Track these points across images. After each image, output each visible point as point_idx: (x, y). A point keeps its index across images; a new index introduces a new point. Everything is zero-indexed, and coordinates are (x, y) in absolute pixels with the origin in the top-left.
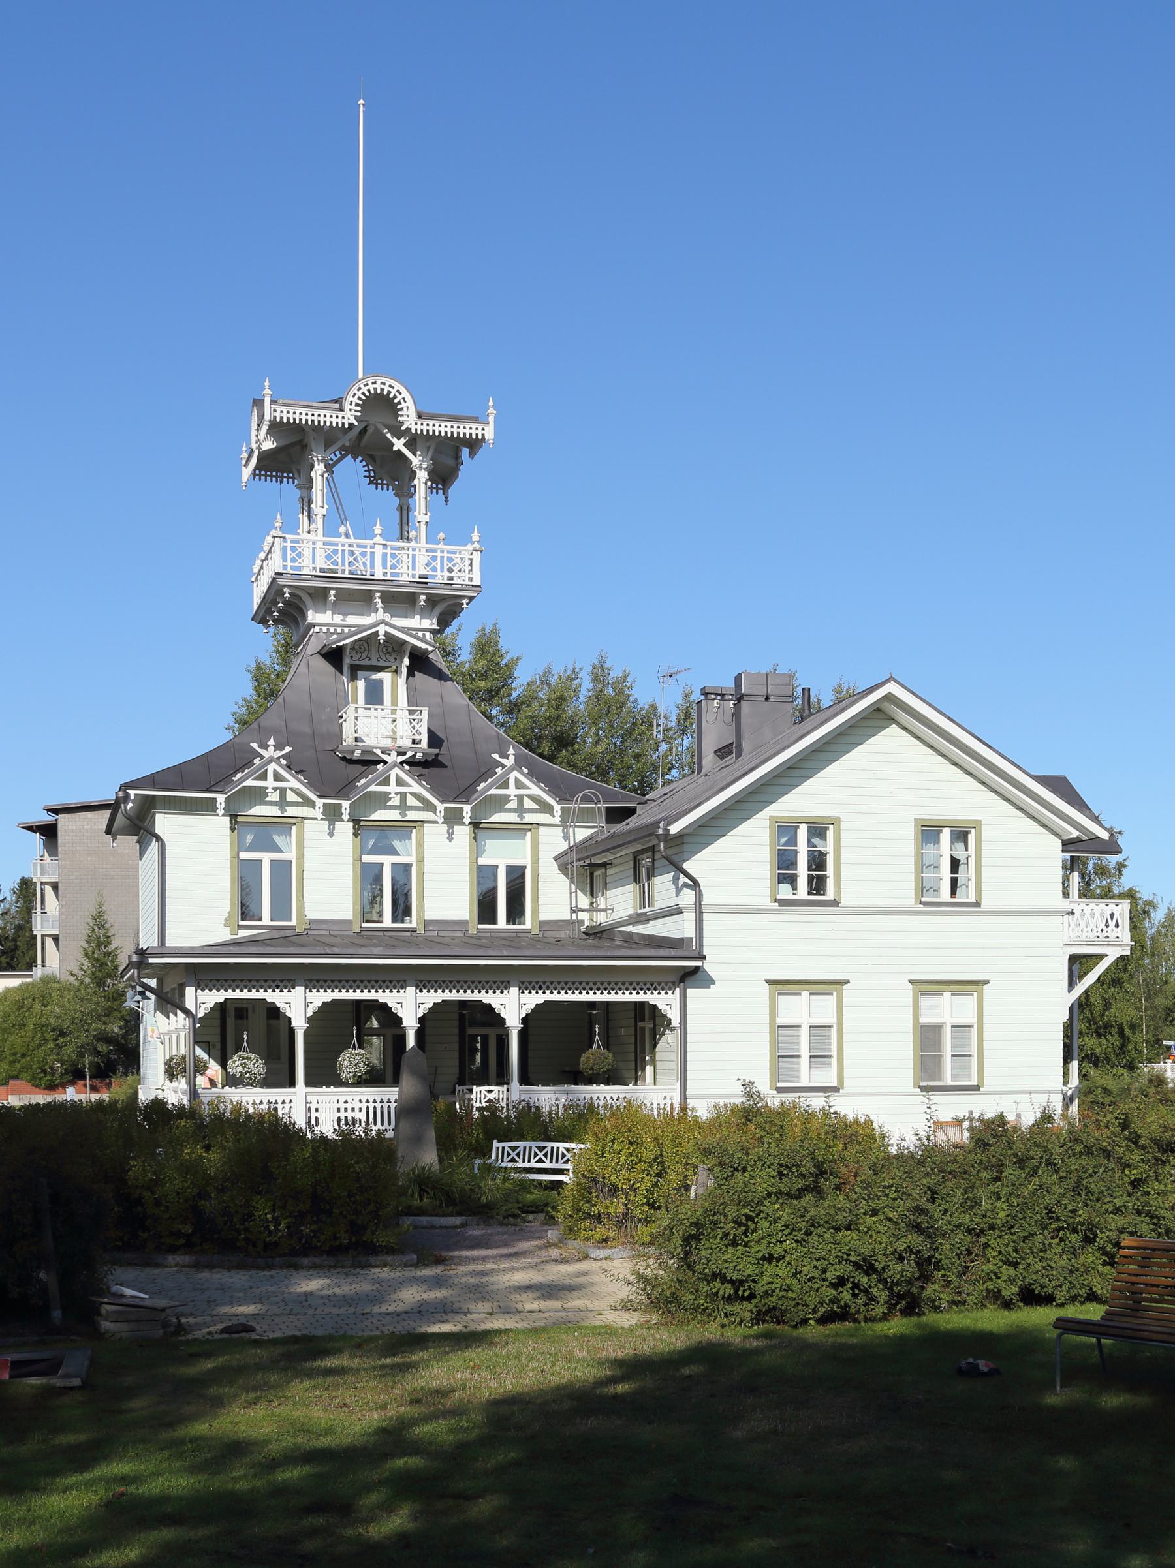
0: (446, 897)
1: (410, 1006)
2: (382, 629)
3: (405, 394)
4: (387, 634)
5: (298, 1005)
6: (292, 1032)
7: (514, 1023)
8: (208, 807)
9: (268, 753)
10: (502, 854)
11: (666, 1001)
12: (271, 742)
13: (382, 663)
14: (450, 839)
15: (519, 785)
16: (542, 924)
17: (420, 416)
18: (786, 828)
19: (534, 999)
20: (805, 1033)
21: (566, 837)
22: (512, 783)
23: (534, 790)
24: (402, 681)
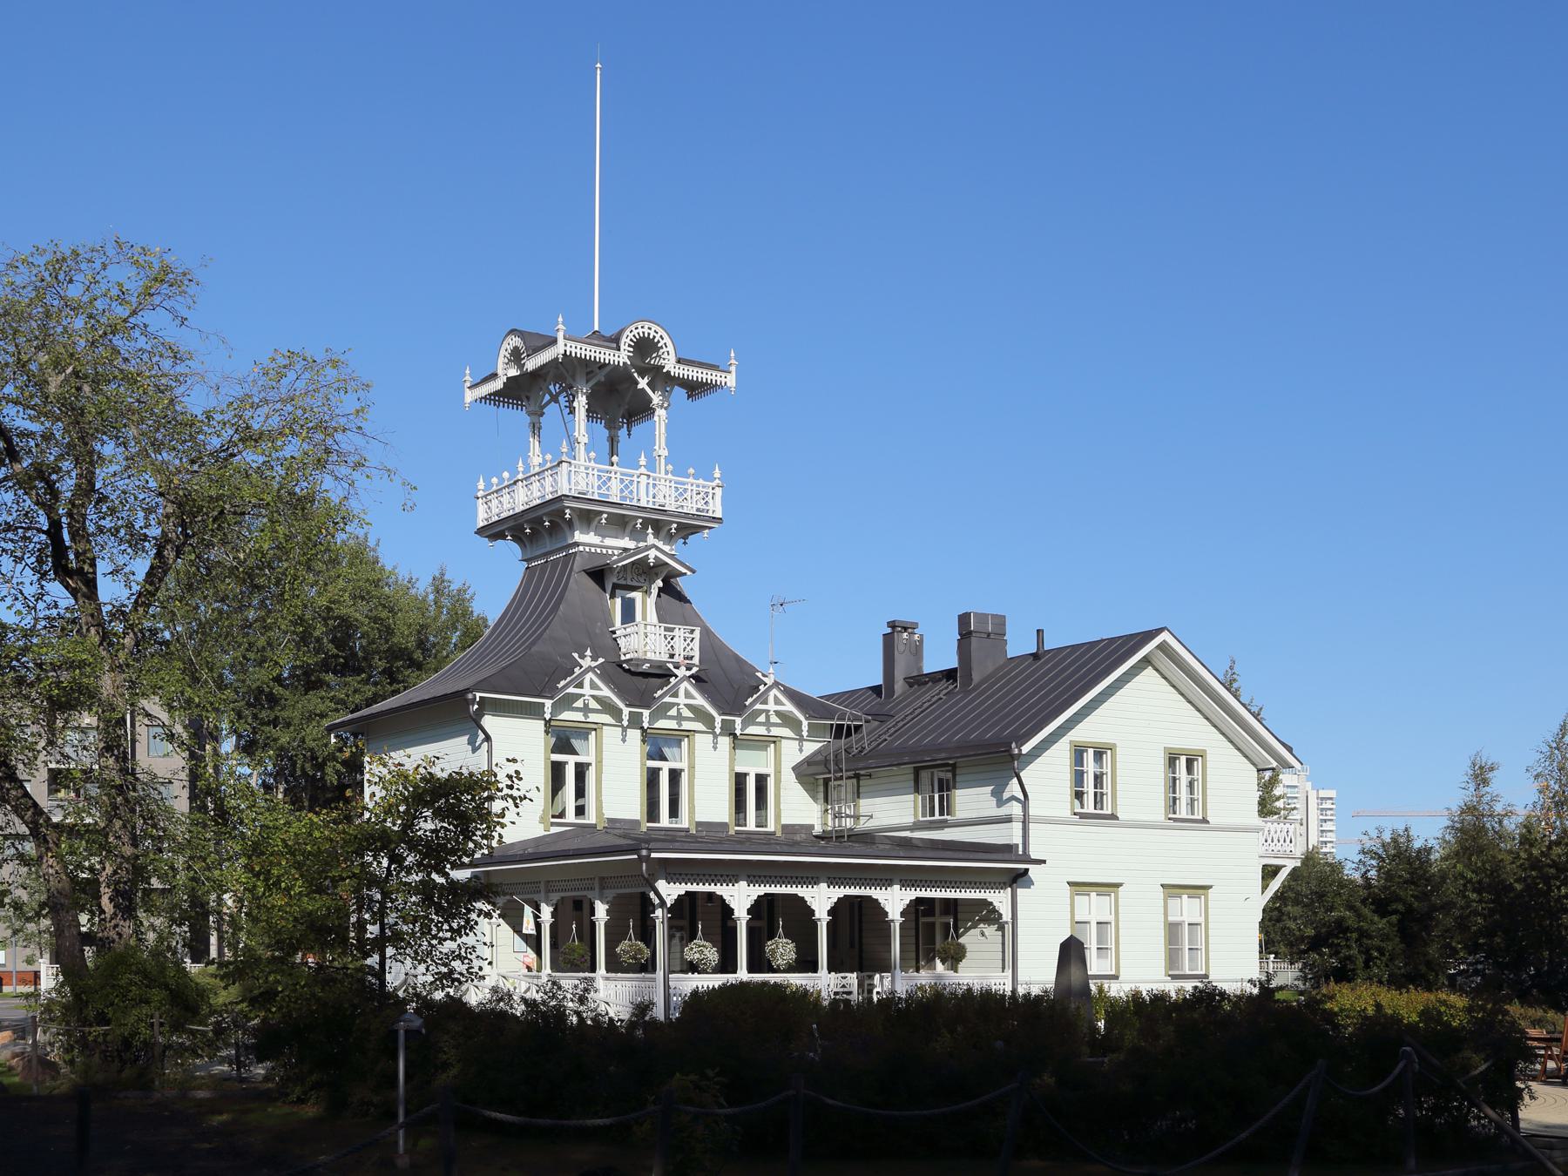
0: (708, 801)
1: (821, 899)
2: (652, 553)
3: (667, 339)
4: (656, 558)
5: (741, 897)
6: (814, 925)
7: (822, 913)
8: (534, 712)
9: (587, 662)
10: (753, 764)
11: (1000, 899)
12: (588, 653)
13: (635, 583)
14: (715, 748)
15: (777, 701)
16: (787, 828)
17: (679, 361)
18: (1078, 753)
19: (912, 894)
20: (1094, 926)
21: (801, 750)
22: (587, 683)
23: (606, 692)
24: (651, 601)
